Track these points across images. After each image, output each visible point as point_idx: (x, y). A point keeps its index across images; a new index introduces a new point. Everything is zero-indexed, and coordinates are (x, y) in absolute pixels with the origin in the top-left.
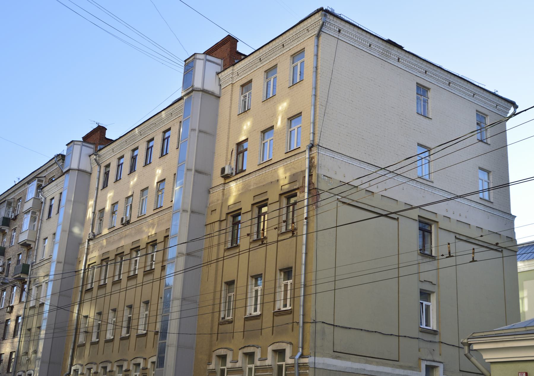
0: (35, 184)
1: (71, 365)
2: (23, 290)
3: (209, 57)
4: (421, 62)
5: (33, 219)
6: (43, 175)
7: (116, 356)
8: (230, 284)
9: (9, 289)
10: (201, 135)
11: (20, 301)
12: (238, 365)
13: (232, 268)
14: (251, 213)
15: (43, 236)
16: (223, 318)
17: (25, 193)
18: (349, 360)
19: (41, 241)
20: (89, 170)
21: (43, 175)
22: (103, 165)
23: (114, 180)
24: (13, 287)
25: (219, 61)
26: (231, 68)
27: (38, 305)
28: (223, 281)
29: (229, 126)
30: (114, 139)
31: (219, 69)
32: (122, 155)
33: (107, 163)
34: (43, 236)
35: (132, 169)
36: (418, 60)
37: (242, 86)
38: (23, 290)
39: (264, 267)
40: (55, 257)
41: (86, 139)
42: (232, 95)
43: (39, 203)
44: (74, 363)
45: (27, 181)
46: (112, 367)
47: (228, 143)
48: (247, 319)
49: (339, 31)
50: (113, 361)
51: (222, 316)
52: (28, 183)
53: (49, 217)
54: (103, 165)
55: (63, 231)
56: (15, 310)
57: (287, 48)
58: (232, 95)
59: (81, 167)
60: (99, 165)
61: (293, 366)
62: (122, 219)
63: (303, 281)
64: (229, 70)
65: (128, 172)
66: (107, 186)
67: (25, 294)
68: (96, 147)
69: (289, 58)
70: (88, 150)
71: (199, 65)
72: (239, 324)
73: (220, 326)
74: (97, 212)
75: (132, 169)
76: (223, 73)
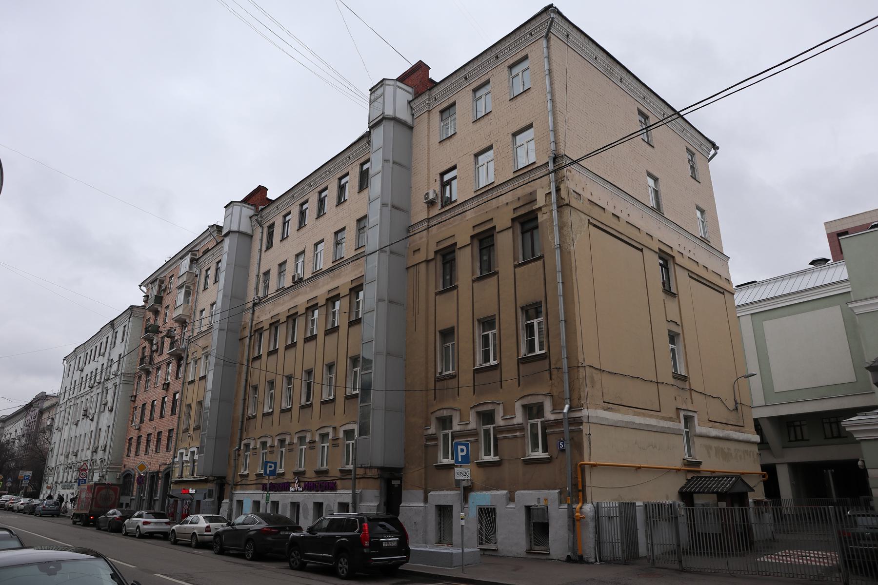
0: (188, 257)
1: (241, 440)
2: (179, 366)
3: (399, 84)
4: (640, 85)
5: (187, 294)
6: (196, 249)
7: (295, 427)
8: (447, 334)
9: (164, 367)
10: (396, 166)
11: (177, 377)
12: (470, 427)
13: (447, 312)
14: (511, 230)
15: (199, 308)
16: (441, 373)
17: (178, 268)
18: (618, 411)
19: (198, 313)
20: (250, 232)
21: (196, 249)
22: (266, 226)
23: (280, 238)
24: (168, 364)
25: (409, 89)
26: (427, 93)
27: (197, 379)
28: (438, 329)
29: (429, 156)
30: (438, 81)
31: (410, 98)
32: (288, 210)
33: (271, 222)
34: (199, 308)
35: (302, 224)
36: (638, 83)
37: (442, 112)
38: (179, 366)
39: (497, 307)
40: (216, 326)
41: (246, 200)
42: (429, 123)
43: (193, 276)
44: (244, 437)
45: (180, 256)
46: (291, 439)
47: (428, 174)
48: (477, 371)
49: (568, 36)
50: (293, 433)
51: (439, 370)
52: (181, 258)
53: (205, 289)
54: (266, 226)
55: (224, 296)
56: (171, 387)
57: (502, 59)
58: (429, 123)
59: (242, 229)
60: (261, 225)
61: (558, 423)
62: (294, 277)
63: (562, 312)
64: (425, 97)
65: (297, 227)
66: (272, 246)
67: (182, 369)
68: (257, 208)
69: (506, 69)
70: (248, 211)
71: (389, 90)
72: (466, 378)
73: (438, 384)
74: (261, 275)
75: (302, 224)
76: (416, 101)
